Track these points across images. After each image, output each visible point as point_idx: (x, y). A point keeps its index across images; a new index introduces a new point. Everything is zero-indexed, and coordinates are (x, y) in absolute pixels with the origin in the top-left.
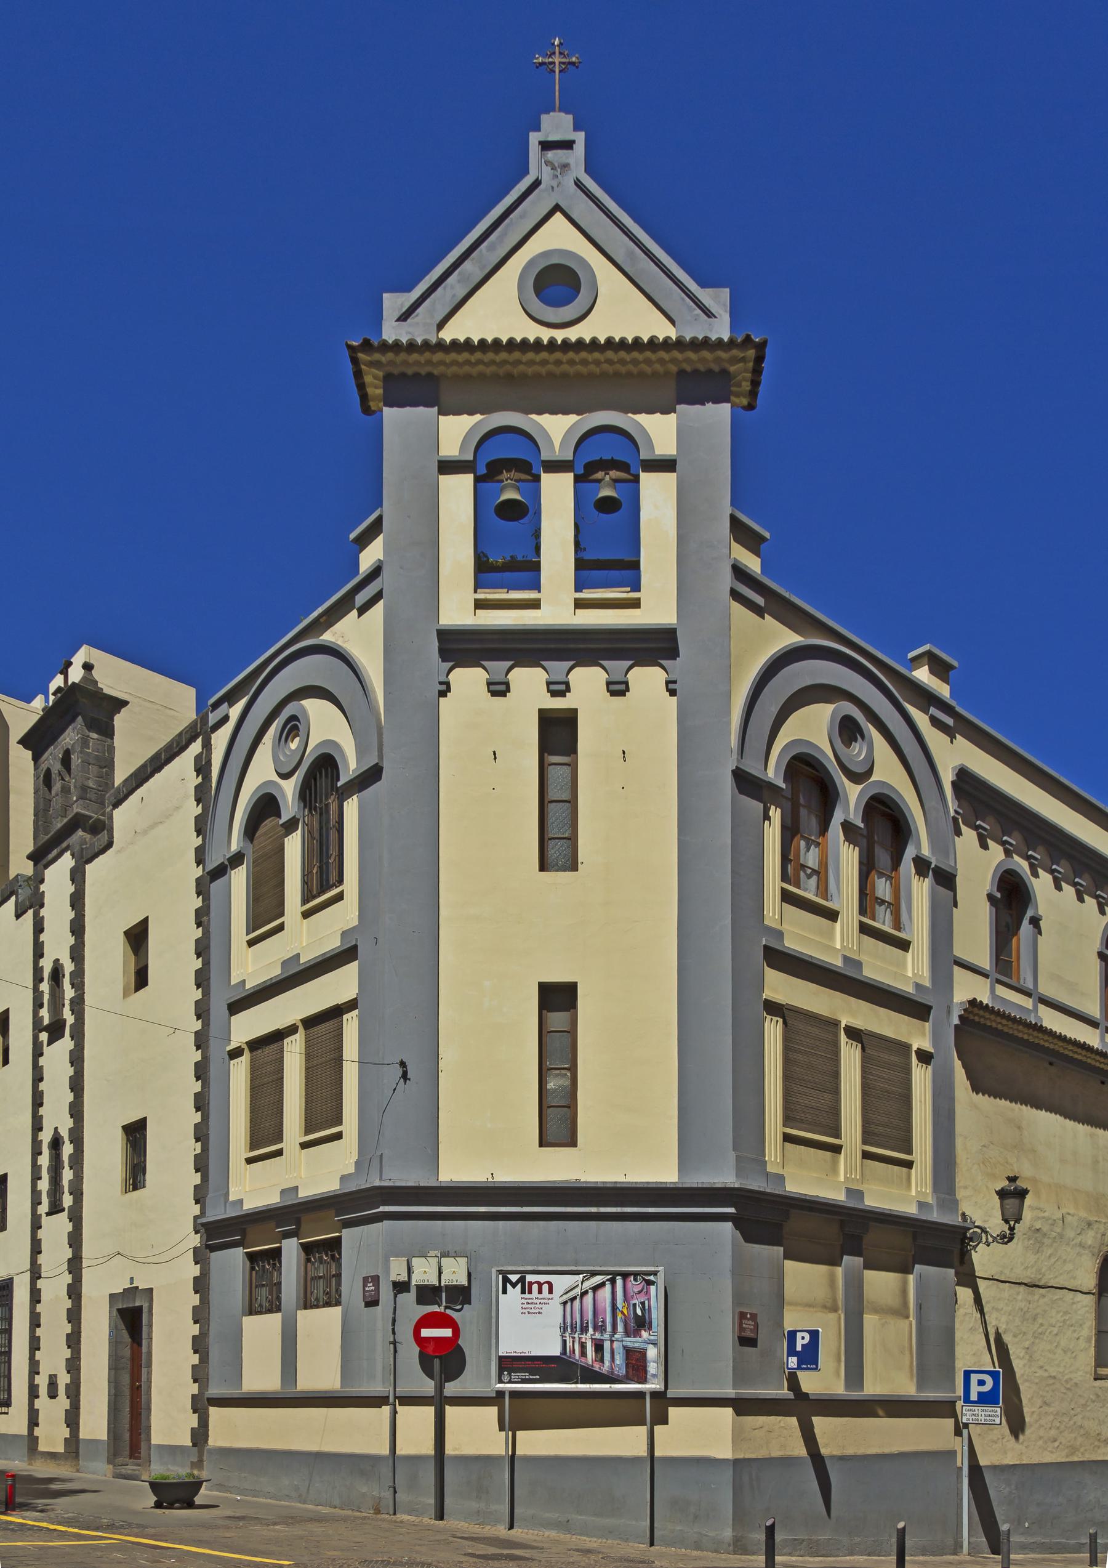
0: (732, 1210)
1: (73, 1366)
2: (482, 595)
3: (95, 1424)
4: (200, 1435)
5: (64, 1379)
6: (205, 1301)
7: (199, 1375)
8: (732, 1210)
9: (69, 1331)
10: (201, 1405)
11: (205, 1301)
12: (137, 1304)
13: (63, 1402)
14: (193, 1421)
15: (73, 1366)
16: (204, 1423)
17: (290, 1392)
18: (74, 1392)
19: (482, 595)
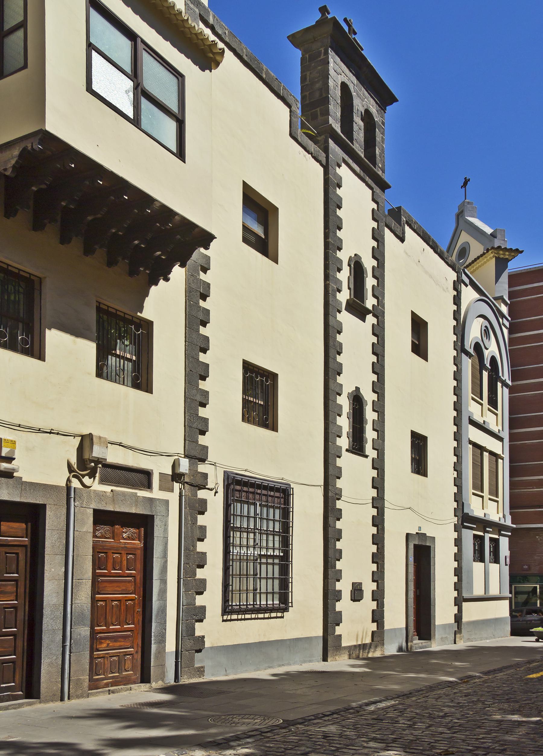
0: (510, 534)
1: (378, 577)
2: (225, 617)
3: (396, 616)
4: (458, 618)
5: (369, 587)
6: (460, 580)
7: (458, 587)
8: (510, 534)
9: (338, 604)
10: (459, 602)
11: (460, 580)
12: (428, 544)
13: (368, 604)
14: (455, 610)
15: (378, 577)
16: (460, 610)
17: (487, 596)
18: (378, 596)
19: (225, 617)
